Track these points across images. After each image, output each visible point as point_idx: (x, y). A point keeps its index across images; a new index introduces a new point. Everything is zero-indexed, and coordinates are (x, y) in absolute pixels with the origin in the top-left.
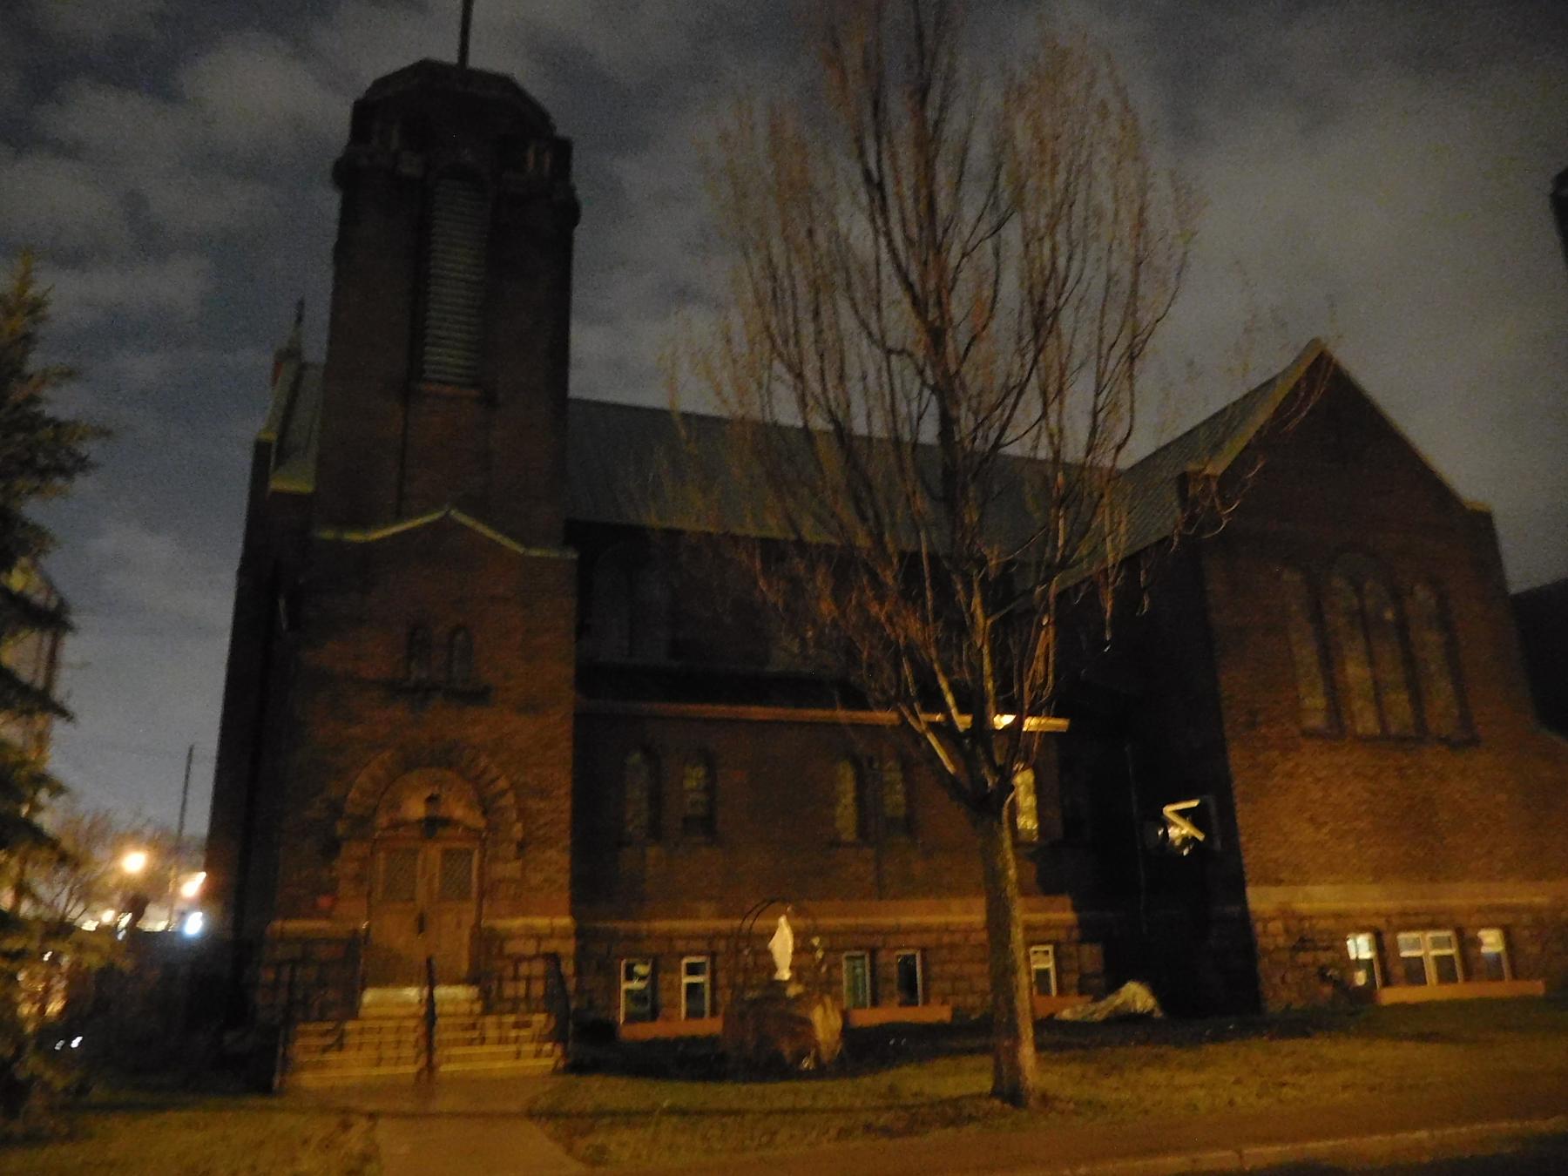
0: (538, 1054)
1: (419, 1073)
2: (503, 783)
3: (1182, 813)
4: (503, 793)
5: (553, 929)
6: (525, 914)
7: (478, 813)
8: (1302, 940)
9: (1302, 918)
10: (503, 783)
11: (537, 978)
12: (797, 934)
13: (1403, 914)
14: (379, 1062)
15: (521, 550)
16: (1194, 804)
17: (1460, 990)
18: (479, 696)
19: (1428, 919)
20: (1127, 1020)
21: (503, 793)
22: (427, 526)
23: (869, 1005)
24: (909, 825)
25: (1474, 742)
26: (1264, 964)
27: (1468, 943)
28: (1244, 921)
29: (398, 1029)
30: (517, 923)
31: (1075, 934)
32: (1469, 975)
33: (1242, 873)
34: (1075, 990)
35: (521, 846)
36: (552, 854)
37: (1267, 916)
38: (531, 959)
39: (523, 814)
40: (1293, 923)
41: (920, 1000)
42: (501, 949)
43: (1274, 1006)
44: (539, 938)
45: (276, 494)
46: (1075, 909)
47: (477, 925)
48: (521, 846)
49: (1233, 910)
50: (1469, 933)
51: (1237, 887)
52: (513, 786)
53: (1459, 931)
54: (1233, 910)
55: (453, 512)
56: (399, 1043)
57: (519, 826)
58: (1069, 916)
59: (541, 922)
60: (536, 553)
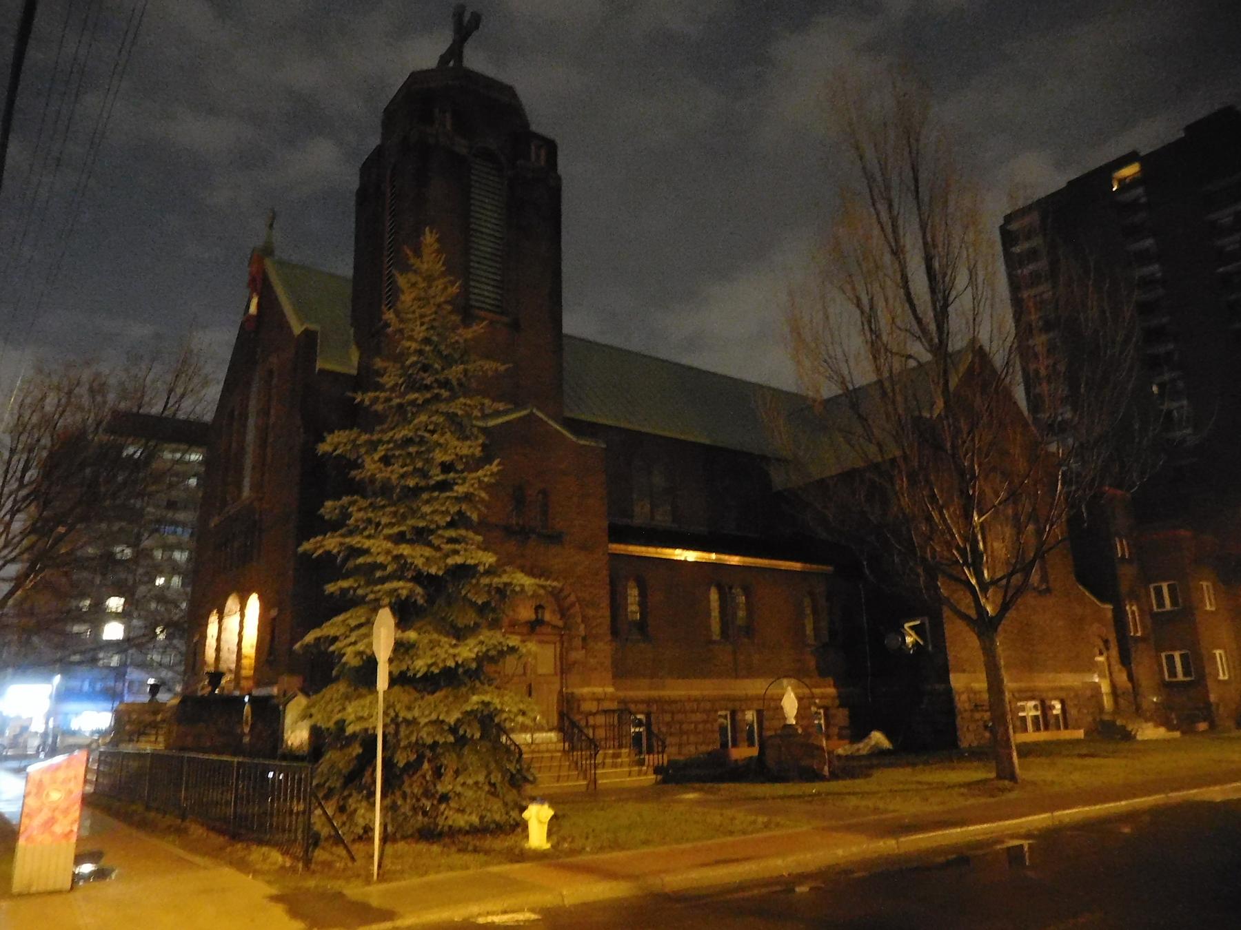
0: (630, 774)
1: (588, 785)
2: (573, 598)
3: (912, 628)
4: (573, 605)
5: (605, 694)
6: (589, 685)
7: (559, 617)
8: (976, 706)
9: (975, 693)
10: (573, 598)
11: (600, 726)
12: (800, 699)
13: (1020, 691)
14: (558, 779)
15: (574, 439)
16: (918, 622)
17: (1043, 736)
18: (555, 538)
19: (1029, 694)
20: (879, 753)
21: (573, 605)
22: (520, 419)
23: (1042, 728)
24: (642, 626)
25: (1048, 590)
26: (959, 720)
27: (1045, 708)
28: (949, 692)
29: (552, 758)
30: (586, 690)
31: (837, 702)
32: (1047, 728)
33: (947, 666)
34: (836, 737)
35: (584, 639)
36: (601, 644)
37: (960, 691)
38: (594, 714)
39: (585, 619)
40: (972, 696)
41: (1042, 728)
42: (579, 707)
43: (964, 744)
44: (599, 700)
45: (322, 371)
46: (835, 686)
47: (561, 692)
48: (584, 639)
49: (940, 687)
50: (1048, 703)
51: (943, 673)
52: (578, 598)
53: (1043, 702)
54: (940, 687)
55: (534, 411)
56: (560, 766)
57: (582, 627)
58: (831, 691)
59: (598, 690)
60: (582, 442)
